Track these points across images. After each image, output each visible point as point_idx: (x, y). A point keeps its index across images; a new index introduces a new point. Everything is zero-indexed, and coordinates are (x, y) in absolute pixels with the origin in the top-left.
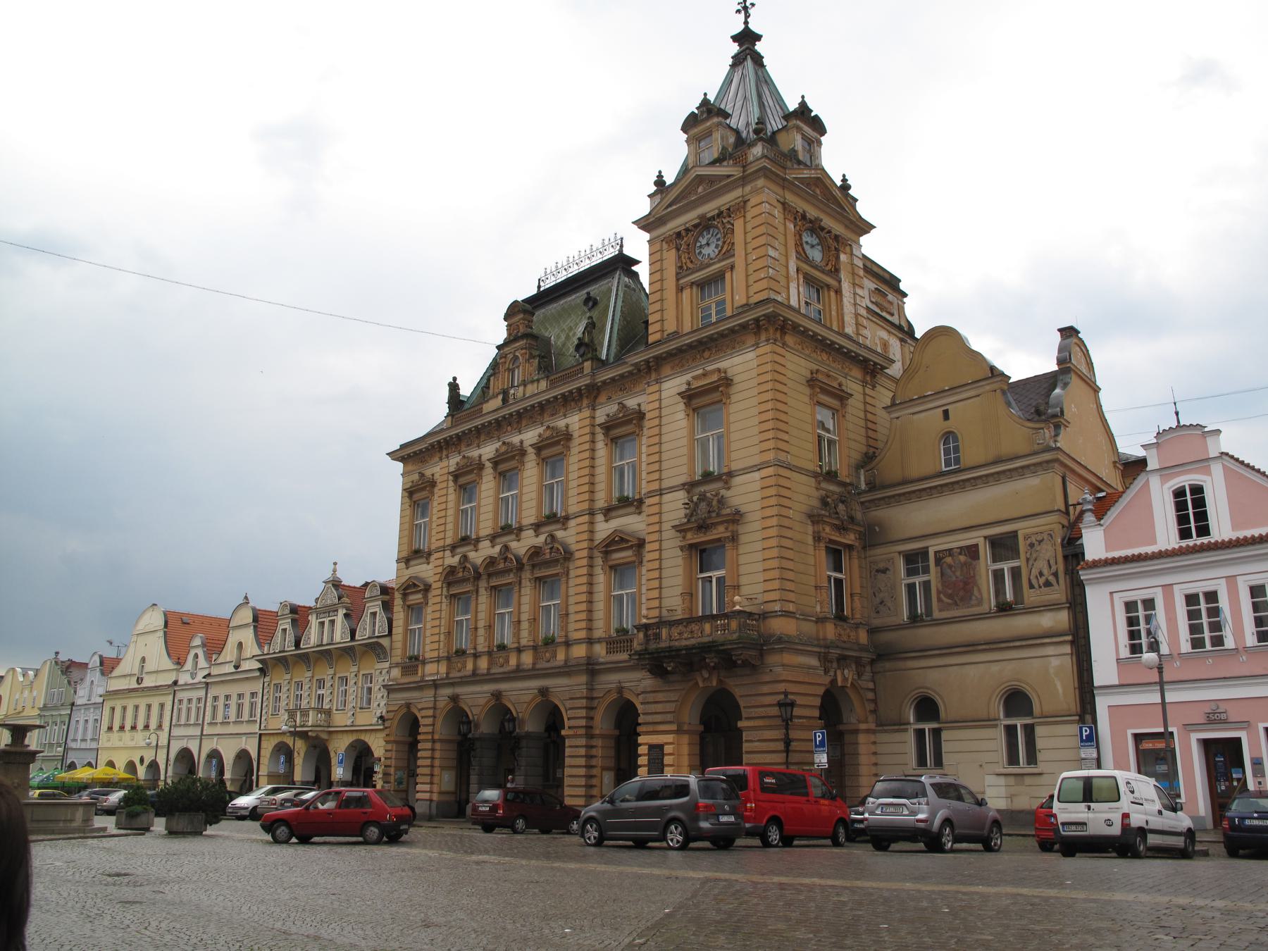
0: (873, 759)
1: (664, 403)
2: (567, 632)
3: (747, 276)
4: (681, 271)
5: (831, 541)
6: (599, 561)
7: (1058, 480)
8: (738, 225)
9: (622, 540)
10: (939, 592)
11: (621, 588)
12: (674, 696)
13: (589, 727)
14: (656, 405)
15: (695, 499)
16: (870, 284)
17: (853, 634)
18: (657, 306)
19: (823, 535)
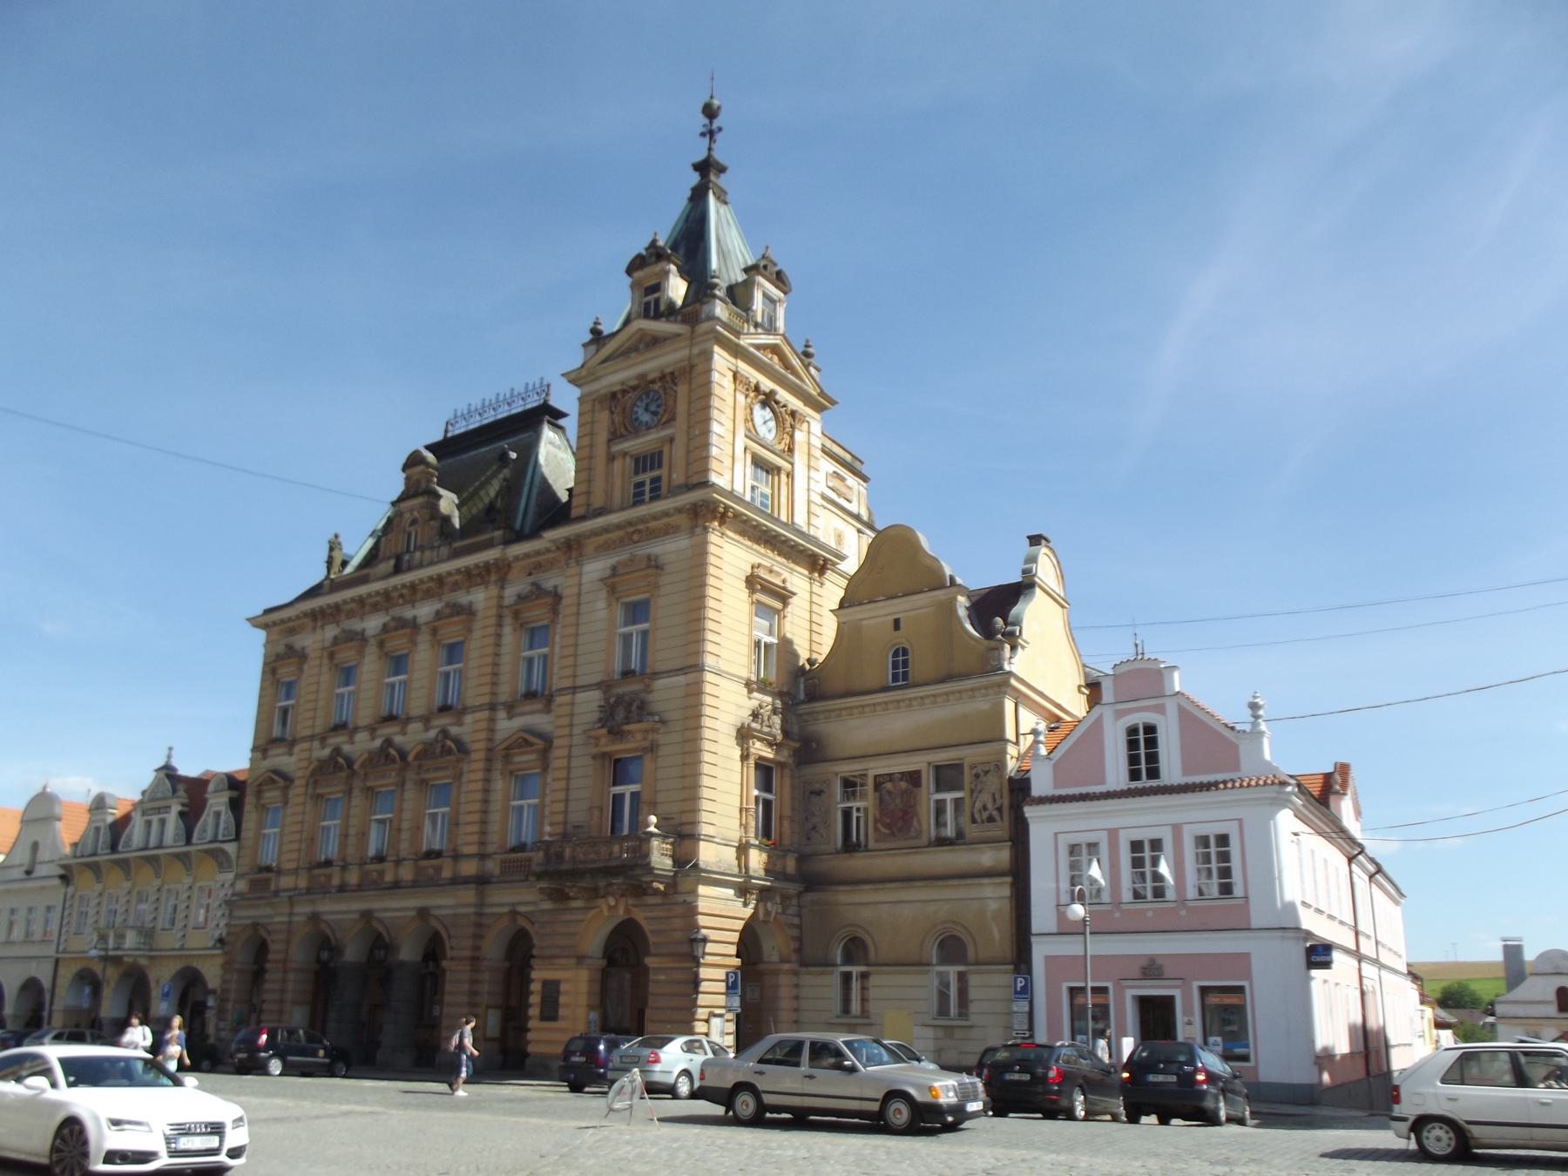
1: (585, 588)
10: (876, 821)
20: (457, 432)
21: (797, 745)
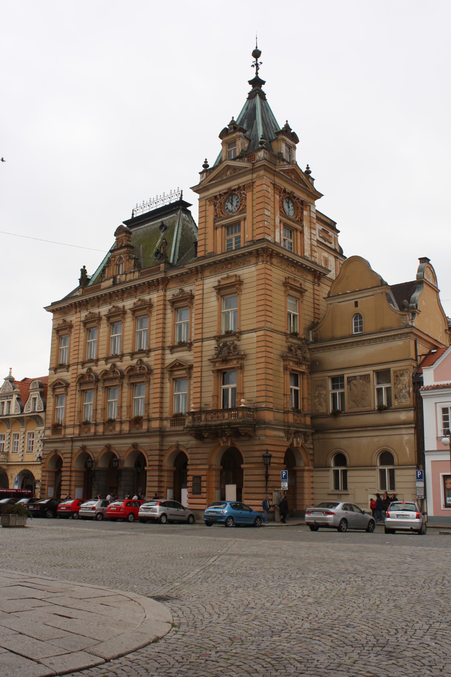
0: (312, 485)
1: (205, 291)
2: (148, 414)
3: (253, 224)
4: (217, 218)
5: (293, 370)
6: (167, 375)
7: (412, 343)
8: (249, 195)
9: (180, 365)
11: (179, 391)
12: (207, 450)
13: (160, 466)
14: (201, 292)
15: (221, 345)
16: (319, 227)
17: (303, 419)
18: (202, 237)
19: (289, 367)
20: (138, 215)
21: (309, 363)
